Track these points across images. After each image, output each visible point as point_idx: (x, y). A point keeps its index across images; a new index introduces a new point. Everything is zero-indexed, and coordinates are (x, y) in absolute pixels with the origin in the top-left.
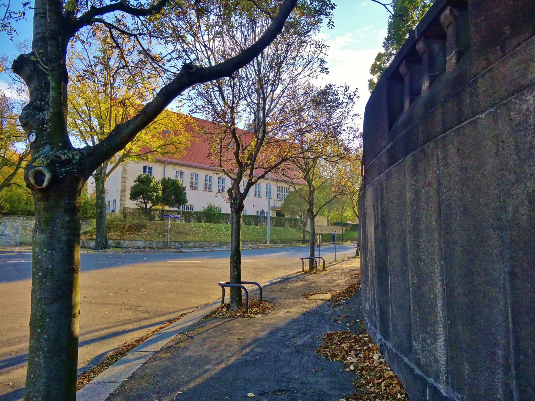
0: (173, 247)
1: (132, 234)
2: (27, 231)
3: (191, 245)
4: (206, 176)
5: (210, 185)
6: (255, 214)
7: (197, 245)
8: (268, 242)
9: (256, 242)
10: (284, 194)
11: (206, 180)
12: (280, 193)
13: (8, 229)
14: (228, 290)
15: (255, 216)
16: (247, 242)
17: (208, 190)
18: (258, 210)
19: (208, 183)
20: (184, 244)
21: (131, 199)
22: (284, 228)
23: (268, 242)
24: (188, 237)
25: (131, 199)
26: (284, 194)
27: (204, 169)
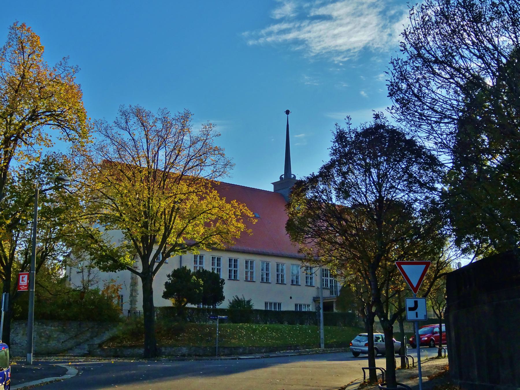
0: (222, 354)
1: (170, 339)
2: (43, 338)
3: (241, 350)
4: (230, 260)
5: (235, 272)
6: (293, 309)
7: (247, 351)
8: (323, 346)
9: (308, 346)
10: (329, 278)
11: (230, 266)
12: (324, 278)
13: (19, 337)
14: (367, 372)
15: (293, 311)
16: (298, 346)
17: (233, 278)
18: (267, 301)
19: (233, 269)
20: (233, 349)
21: (163, 297)
22: (337, 328)
23: (323, 346)
24: (233, 341)
25: (163, 297)
26: (329, 278)
27: (244, 252)
